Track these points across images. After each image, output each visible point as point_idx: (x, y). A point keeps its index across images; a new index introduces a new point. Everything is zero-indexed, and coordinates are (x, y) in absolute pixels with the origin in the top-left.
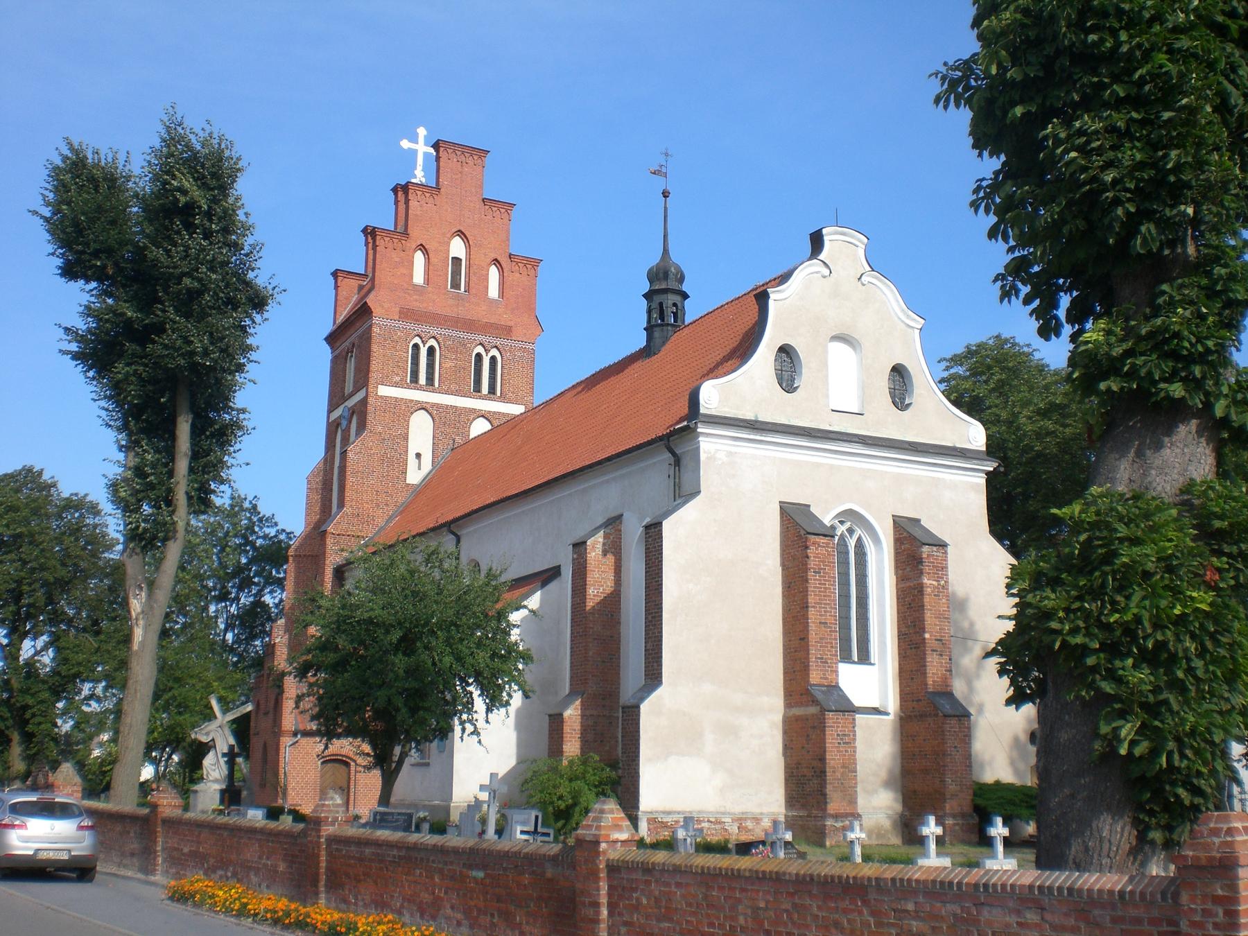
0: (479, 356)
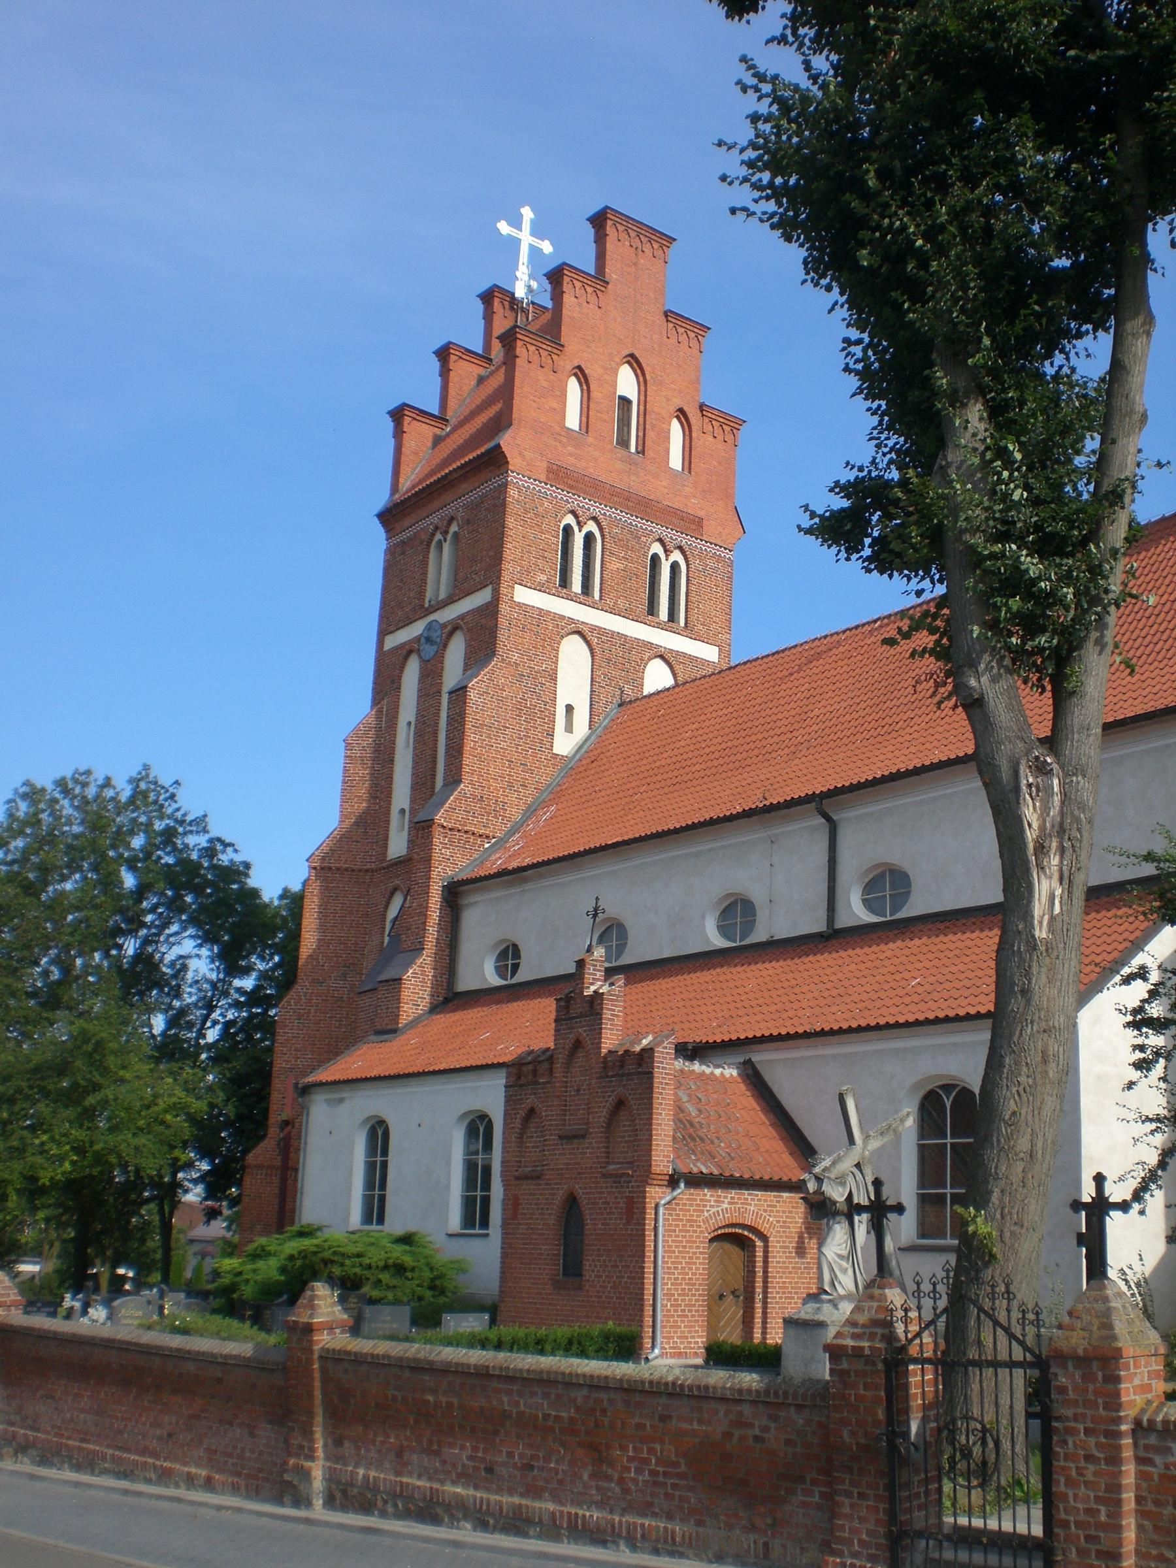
0: (655, 559)
